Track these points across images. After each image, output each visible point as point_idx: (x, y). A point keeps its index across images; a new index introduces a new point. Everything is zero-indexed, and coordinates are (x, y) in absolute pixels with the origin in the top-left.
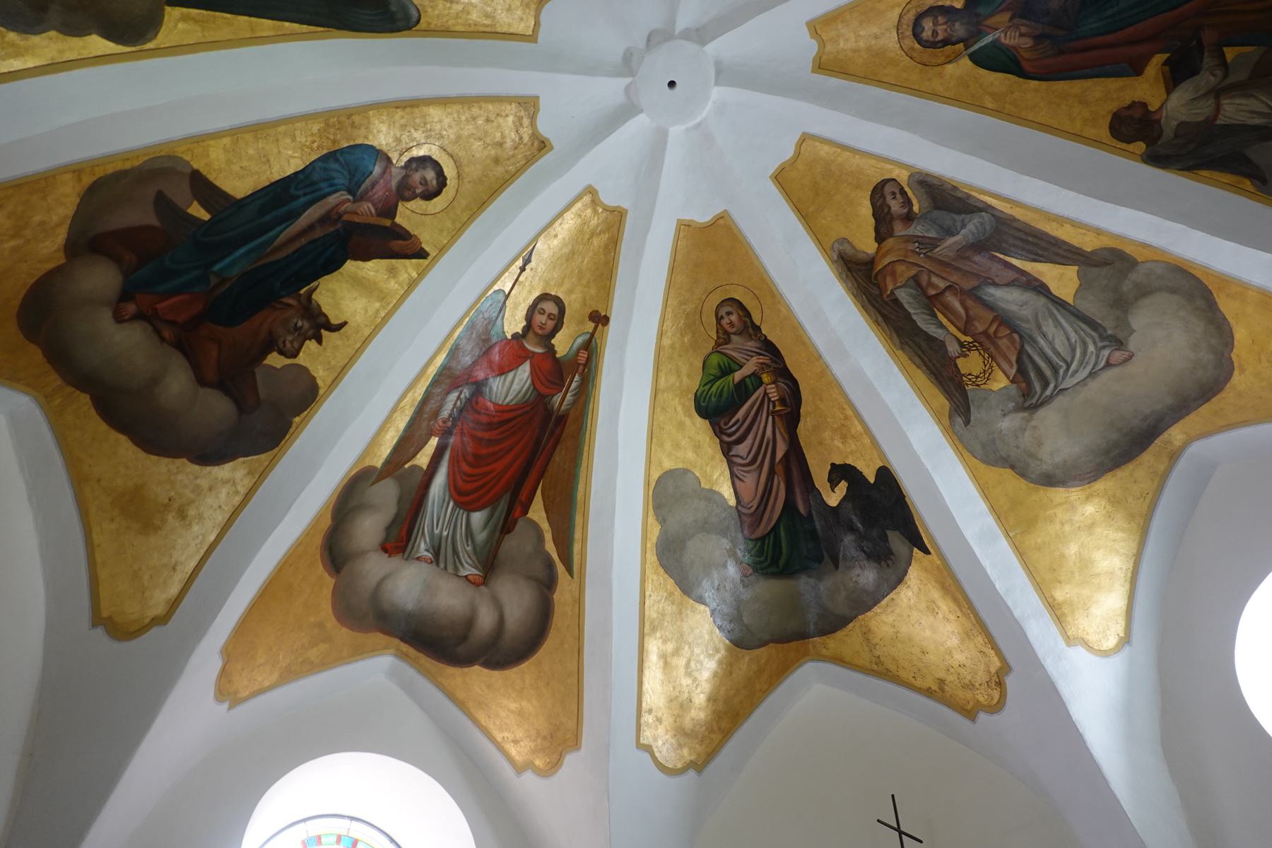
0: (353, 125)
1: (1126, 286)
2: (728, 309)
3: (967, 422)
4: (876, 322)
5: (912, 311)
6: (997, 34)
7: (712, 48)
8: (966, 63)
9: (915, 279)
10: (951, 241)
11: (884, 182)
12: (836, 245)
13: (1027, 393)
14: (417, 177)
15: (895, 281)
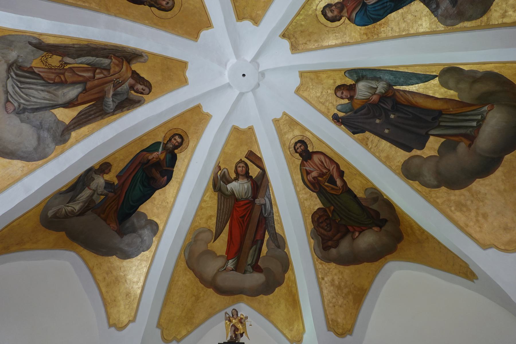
0: (366, 34)
1: (45, 134)
2: (169, 5)
3: (30, 43)
4: (107, 45)
5: (97, 59)
6: (160, 153)
7: (237, 92)
8: (160, 140)
9: (109, 70)
10: (111, 93)
11: (150, 91)
12: (146, 58)
13: (20, 68)
14: (336, 13)
15: (115, 64)
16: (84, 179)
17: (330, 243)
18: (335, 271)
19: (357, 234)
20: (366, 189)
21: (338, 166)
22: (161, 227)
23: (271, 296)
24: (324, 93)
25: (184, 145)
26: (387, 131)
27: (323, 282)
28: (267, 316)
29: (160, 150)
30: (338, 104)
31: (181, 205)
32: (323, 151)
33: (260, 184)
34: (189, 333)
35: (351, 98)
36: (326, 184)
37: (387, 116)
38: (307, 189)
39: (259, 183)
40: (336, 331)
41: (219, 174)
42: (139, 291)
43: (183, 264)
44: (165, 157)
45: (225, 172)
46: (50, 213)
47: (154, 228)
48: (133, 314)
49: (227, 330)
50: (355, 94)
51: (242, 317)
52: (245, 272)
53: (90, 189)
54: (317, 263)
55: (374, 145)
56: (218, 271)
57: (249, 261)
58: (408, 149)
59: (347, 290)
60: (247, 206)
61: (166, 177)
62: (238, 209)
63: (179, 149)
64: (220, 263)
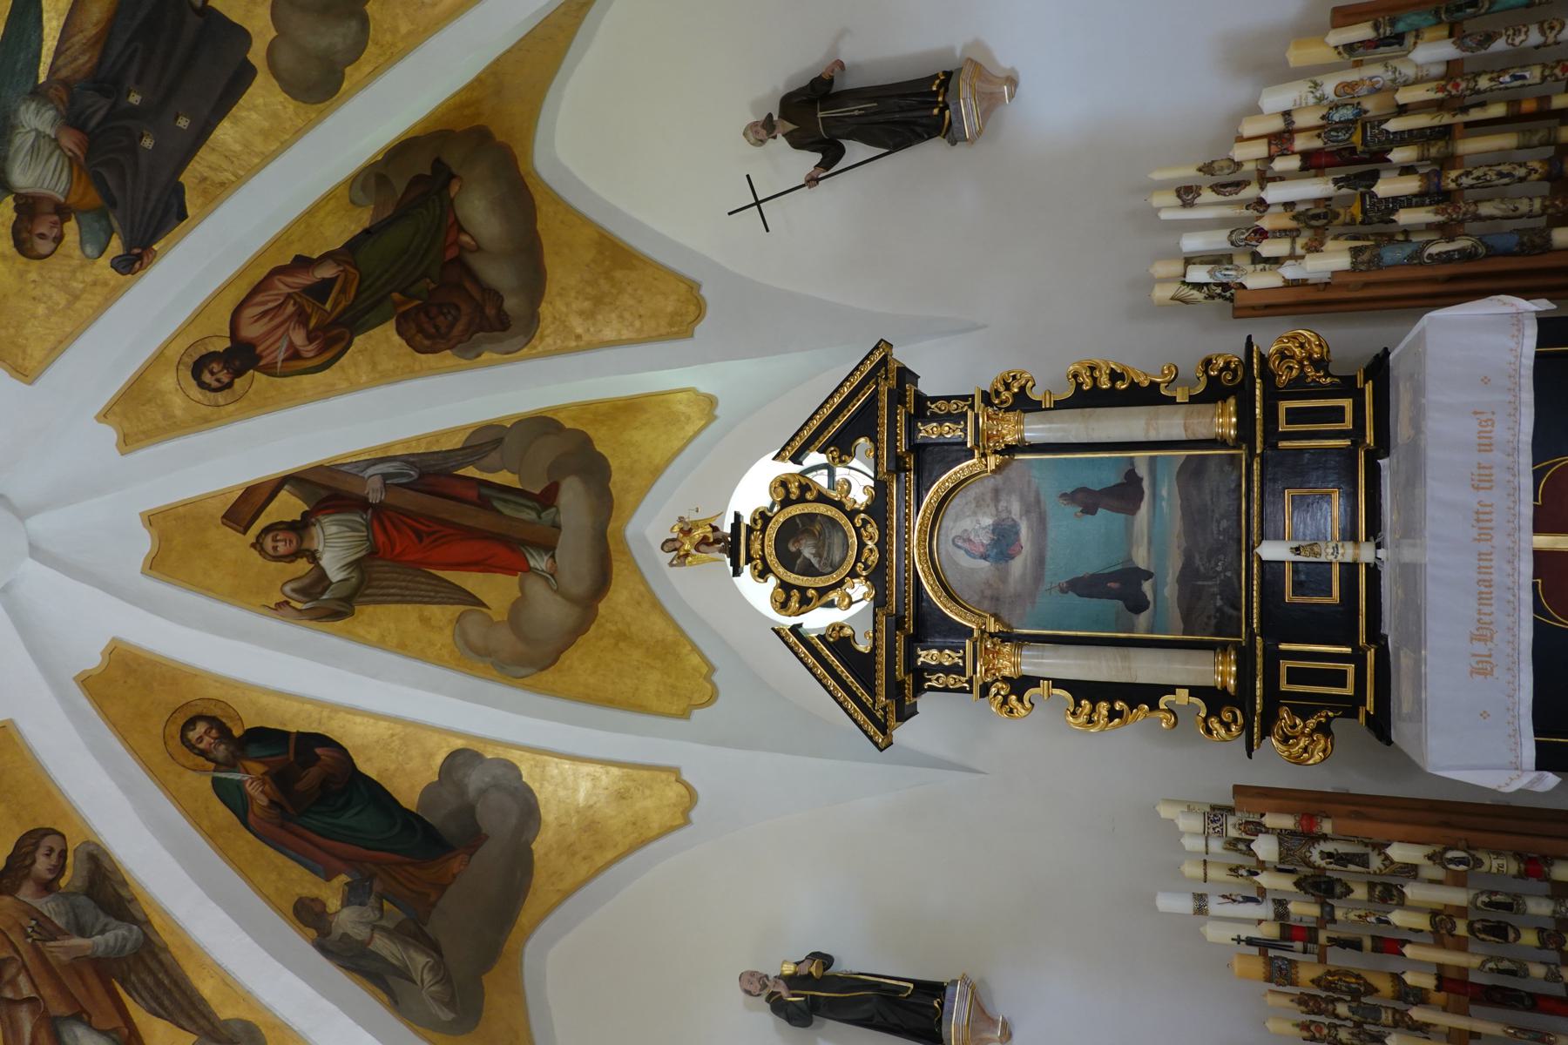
8: (205, 782)
10: (77, 941)
16: (350, 956)
17: (490, 311)
18: (560, 305)
19: (465, 238)
20: (352, 202)
21: (279, 271)
22: (459, 744)
23: (614, 464)
24: (37, 293)
25: (216, 712)
26: (183, 123)
27: (586, 338)
28: (657, 472)
29: (236, 776)
30: (78, 253)
31: (391, 697)
32: (232, 308)
33: (325, 490)
34: (695, 648)
35: (63, 212)
36: (328, 306)
37: (134, 112)
38: (344, 360)
39: (324, 494)
40: (692, 318)
41: (299, 606)
42: (615, 771)
43: (548, 676)
44: (257, 759)
45: (294, 590)
46: (446, 1015)
47: (461, 760)
48: (664, 776)
49: (704, 562)
50: (50, 199)
51: (676, 529)
52: (557, 527)
53: (372, 937)
54: (540, 348)
55: (225, 164)
56: (556, 592)
57: (530, 515)
58: (244, 75)
59: (602, 281)
60: (387, 524)
61: (318, 751)
62: (398, 549)
63: (229, 724)
64: (537, 589)
